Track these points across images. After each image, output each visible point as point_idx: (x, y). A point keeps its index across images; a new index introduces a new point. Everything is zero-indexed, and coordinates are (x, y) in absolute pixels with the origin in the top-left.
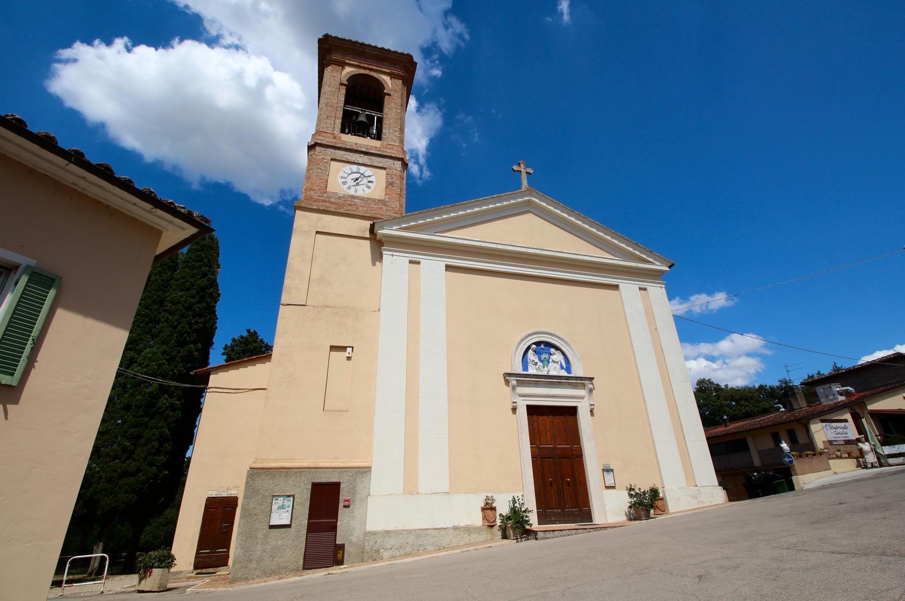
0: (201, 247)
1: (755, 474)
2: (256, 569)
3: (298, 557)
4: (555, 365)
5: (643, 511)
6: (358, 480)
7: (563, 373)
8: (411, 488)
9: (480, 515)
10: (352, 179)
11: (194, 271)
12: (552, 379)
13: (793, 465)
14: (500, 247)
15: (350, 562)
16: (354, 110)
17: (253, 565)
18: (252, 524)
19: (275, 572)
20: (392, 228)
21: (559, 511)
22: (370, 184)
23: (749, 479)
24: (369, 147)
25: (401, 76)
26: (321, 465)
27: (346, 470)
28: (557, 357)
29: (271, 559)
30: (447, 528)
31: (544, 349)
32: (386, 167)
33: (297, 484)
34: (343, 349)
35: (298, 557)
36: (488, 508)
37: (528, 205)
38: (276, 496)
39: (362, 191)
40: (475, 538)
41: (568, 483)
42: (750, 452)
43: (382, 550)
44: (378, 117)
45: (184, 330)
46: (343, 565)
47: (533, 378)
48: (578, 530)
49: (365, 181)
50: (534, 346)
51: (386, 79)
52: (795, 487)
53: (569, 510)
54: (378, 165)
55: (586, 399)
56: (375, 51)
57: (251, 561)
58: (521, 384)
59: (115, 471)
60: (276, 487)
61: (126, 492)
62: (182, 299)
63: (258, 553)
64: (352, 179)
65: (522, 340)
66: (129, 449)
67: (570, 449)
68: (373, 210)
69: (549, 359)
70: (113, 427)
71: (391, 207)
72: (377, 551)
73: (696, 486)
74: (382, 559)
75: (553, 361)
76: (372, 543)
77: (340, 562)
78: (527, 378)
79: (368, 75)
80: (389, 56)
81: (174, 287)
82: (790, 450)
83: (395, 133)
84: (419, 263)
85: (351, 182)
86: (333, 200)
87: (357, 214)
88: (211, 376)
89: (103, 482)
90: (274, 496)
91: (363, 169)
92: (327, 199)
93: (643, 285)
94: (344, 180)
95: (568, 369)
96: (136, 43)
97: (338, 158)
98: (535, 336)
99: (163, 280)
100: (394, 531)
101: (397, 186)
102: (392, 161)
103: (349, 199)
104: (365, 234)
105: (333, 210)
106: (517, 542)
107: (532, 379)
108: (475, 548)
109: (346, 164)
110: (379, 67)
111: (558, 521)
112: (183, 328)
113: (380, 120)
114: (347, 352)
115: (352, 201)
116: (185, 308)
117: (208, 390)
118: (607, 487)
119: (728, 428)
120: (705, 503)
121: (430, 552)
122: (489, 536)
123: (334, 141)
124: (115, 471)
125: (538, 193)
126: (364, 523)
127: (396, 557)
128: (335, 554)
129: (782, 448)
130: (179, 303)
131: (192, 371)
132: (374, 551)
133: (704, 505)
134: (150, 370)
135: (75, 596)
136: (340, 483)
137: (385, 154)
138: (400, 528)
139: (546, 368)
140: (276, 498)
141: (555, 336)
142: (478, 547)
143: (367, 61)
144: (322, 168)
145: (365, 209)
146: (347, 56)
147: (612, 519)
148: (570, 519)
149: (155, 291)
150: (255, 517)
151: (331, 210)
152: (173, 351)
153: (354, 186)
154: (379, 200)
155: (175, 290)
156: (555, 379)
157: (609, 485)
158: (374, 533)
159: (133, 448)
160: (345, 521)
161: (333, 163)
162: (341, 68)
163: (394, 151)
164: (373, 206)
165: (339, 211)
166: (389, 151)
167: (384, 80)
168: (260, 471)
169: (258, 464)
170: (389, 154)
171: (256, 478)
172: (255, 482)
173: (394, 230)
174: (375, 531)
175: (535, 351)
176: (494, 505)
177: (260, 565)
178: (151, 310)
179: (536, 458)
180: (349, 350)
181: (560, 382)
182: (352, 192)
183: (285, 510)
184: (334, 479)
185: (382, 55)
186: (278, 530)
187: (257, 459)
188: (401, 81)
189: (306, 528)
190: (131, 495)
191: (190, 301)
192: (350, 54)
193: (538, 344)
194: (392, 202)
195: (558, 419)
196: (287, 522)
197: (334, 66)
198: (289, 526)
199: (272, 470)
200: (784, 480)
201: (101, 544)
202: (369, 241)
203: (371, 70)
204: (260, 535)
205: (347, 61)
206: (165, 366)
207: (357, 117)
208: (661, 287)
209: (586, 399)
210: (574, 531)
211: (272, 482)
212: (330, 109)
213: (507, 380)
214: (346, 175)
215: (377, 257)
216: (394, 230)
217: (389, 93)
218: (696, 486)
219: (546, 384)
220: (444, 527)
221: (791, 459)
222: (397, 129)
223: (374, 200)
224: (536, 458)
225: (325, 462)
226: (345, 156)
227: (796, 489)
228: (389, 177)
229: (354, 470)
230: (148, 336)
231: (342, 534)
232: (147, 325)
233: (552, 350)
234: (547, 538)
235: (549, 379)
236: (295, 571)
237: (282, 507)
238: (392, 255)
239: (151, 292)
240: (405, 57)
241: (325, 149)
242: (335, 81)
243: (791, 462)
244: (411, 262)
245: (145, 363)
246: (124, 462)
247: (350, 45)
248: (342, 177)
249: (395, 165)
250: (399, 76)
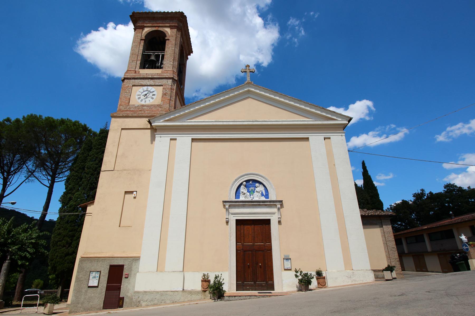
0: (101, 137)
1: (458, 255)
2: (81, 307)
3: (101, 302)
4: (257, 194)
5: (303, 286)
6: (133, 264)
7: (263, 199)
8: (160, 268)
9: (200, 283)
10: (143, 95)
11: (98, 151)
12: (254, 203)
13: (469, 251)
14: (225, 123)
15: (126, 307)
16: (149, 53)
17: (80, 305)
18: (80, 285)
19: (89, 310)
20: (160, 121)
21: (252, 283)
22: (153, 96)
23: (453, 258)
24: (154, 74)
25: (176, 27)
26: (116, 255)
27: (128, 258)
28: (260, 188)
29: (88, 303)
30: (179, 291)
31: (251, 184)
32: (163, 84)
33: (103, 266)
34: (132, 192)
35: (101, 302)
36: (205, 280)
37: (249, 93)
38: (92, 271)
39: (149, 101)
40: (194, 297)
41: (261, 267)
42: (455, 240)
43: (142, 301)
44: (162, 55)
45: (93, 182)
46: (122, 308)
47: (241, 203)
48: (252, 297)
49: (151, 94)
50: (245, 183)
51: (168, 30)
52: (470, 268)
53: (259, 282)
54: (158, 84)
55: (277, 214)
56: (160, 15)
57: (78, 303)
58: (235, 206)
59: (63, 253)
60: (92, 267)
61: (68, 263)
62: (92, 166)
63: (82, 299)
64: (143, 95)
65: (236, 180)
66: (69, 242)
67: (264, 245)
68: (153, 112)
69: (255, 190)
70: (62, 232)
71: (164, 108)
72: (139, 302)
73: (353, 270)
74: (141, 306)
75: (257, 192)
76: (137, 297)
77: (121, 306)
78: (237, 203)
79: (157, 30)
80: (168, 16)
81: (89, 160)
82: (468, 241)
83: (170, 63)
84: (176, 139)
85: (142, 97)
86: (132, 109)
87: (143, 115)
88: (88, 208)
89: (58, 258)
90: (91, 272)
91: (150, 88)
92: (129, 109)
93: (327, 135)
94: (139, 96)
95: (267, 196)
96: (117, 24)
97: (136, 85)
98: (246, 177)
99: (84, 157)
100: (149, 291)
101: (168, 95)
102: (167, 80)
103: (141, 107)
104: (147, 126)
105: (131, 115)
106: (215, 301)
107: (240, 204)
108: (189, 303)
109: (141, 87)
110: (163, 24)
111: (251, 289)
112: (92, 180)
113: (163, 56)
114: (134, 194)
115: (142, 108)
116: (93, 170)
117: (86, 215)
118: (285, 270)
119: (453, 220)
120: (357, 281)
121: (169, 304)
122: (203, 297)
123: (135, 74)
124: (63, 253)
125: (240, 87)
126: (134, 287)
127: (149, 305)
128: (119, 302)
129: (461, 239)
130: (91, 168)
131: (78, 206)
132: (137, 302)
133: (356, 283)
134: (77, 203)
135: (26, 314)
136: (124, 265)
137: (162, 77)
138: (153, 290)
139: (252, 196)
140: (92, 272)
141: (259, 175)
142: (191, 303)
143: (156, 22)
144: (127, 92)
145: (149, 112)
146: (146, 22)
147: (285, 290)
148: (259, 288)
149: (80, 163)
150: (82, 282)
151: (129, 115)
152: (88, 193)
153: (145, 99)
154: (157, 105)
155: (89, 161)
156: (255, 203)
157: (287, 268)
158: (138, 292)
159: (71, 241)
160: (125, 285)
161: (133, 87)
162: (142, 30)
163: (168, 74)
164: (154, 109)
165: (134, 115)
166: (165, 74)
167: (166, 31)
168: (85, 259)
169: (84, 255)
170: (164, 77)
171: (83, 262)
172: (82, 264)
173: (161, 122)
174: (138, 291)
175: (246, 186)
176: (209, 279)
177: (83, 306)
178: (78, 173)
179: (241, 251)
180: (135, 193)
181: (259, 204)
182: (143, 103)
183: (96, 279)
184: (121, 263)
185: (164, 16)
186: (92, 288)
187: (85, 253)
188: (176, 29)
189: (106, 288)
190: (70, 264)
191: (95, 167)
192: (147, 21)
193: (247, 181)
194: (165, 105)
195: (258, 227)
196: (96, 285)
197: (138, 30)
198: (97, 287)
199: (91, 258)
200: (464, 262)
201: (60, 287)
202: (150, 130)
203: (159, 27)
204: (83, 291)
205: (145, 25)
206: (84, 201)
207: (150, 58)
208: (342, 135)
209: (277, 214)
210: (249, 297)
211: (90, 264)
212: (134, 56)
213: (224, 205)
214: (140, 93)
215: (153, 139)
216: (161, 122)
217: (168, 38)
218: (353, 270)
219: (250, 206)
220: (177, 290)
221: (467, 247)
222: (172, 60)
223: (154, 106)
224: (241, 251)
225: (117, 254)
226: (140, 83)
227: (471, 270)
228: (164, 90)
229: (131, 258)
230: (77, 186)
231: (123, 292)
232: (77, 180)
233: (257, 185)
234: (230, 300)
235: (251, 203)
236: (99, 309)
237: (95, 277)
238: (161, 137)
239: (78, 164)
240: (178, 14)
241: (130, 80)
242: (138, 38)
243: (467, 249)
244: (171, 139)
245: (75, 200)
246: (67, 248)
247: (146, 15)
248: (138, 95)
249: (168, 82)
250: (175, 27)
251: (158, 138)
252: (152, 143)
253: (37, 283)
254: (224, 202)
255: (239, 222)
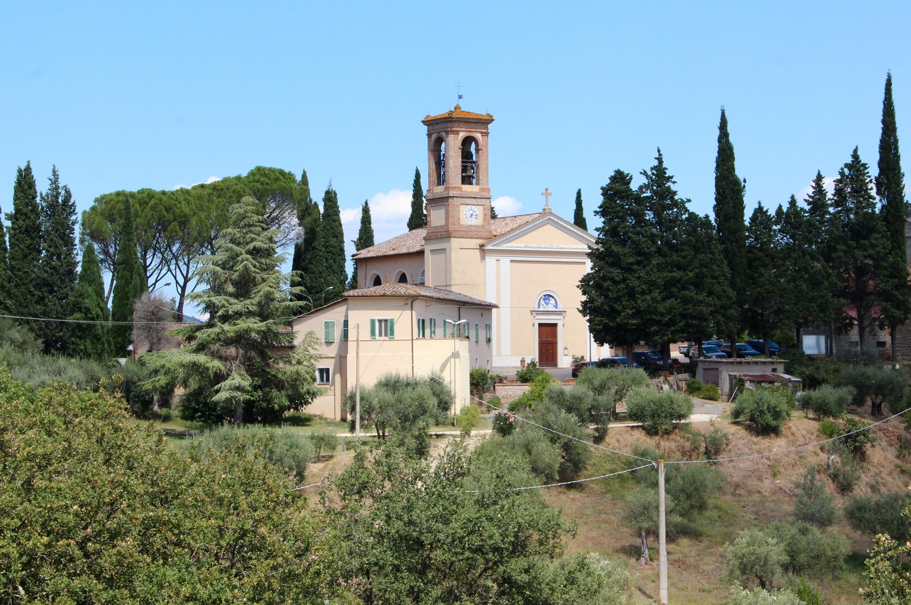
7: (554, 309)
95: (556, 307)
195: (549, 328)
251: (487, 259)
252: (793, 197)
253: (280, 376)
254: (531, 311)
255: (540, 325)
